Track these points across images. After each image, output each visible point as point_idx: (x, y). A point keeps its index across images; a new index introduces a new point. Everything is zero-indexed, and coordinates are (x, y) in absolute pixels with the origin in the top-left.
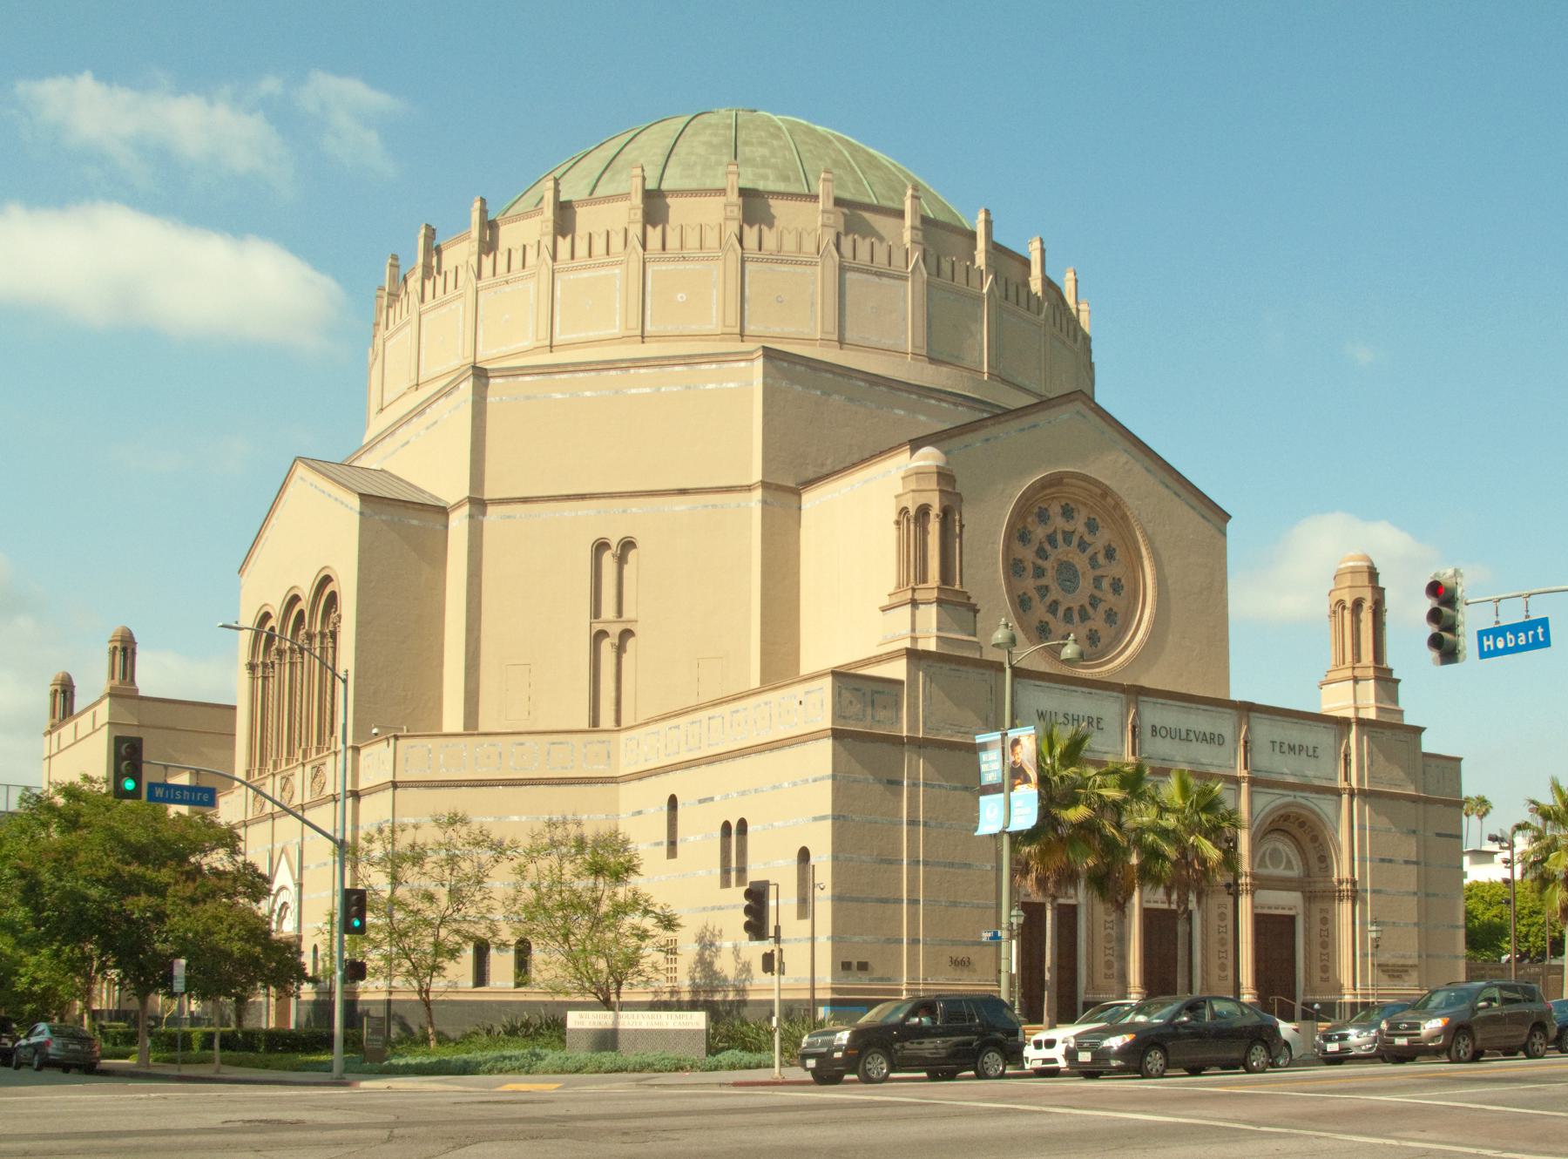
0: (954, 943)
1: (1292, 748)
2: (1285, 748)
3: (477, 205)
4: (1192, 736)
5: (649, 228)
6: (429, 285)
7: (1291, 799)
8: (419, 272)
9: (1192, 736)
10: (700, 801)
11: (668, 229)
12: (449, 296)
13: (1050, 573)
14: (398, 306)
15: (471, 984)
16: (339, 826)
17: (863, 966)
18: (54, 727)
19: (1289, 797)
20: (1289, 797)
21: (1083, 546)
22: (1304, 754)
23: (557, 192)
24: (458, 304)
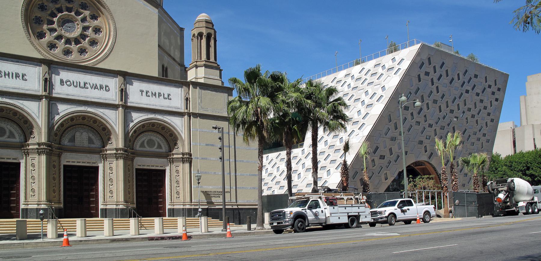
2: (150, 94)
4: (88, 85)
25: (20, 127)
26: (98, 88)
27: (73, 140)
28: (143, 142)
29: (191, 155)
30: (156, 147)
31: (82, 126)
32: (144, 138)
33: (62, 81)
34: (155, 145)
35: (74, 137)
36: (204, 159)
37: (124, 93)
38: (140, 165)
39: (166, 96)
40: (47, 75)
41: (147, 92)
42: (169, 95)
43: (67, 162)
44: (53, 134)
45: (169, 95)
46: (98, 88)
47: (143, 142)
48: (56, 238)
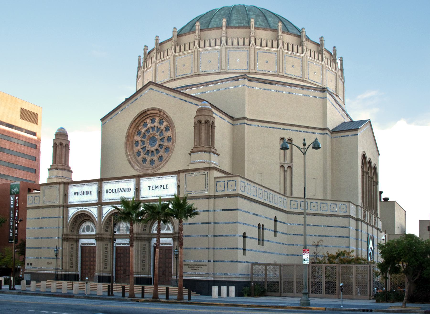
1: (157, 187)
2: (154, 187)
4: (120, 190)
7: (81, 210)
9: (120, 190)
10: (223, 210)
12: (165, 58)
13: (158, 143)
17: (31, 264)
18: (193, 204)
19: (81, 209)
20: (81, 209)
22: (162, 188)
35: (119, 227)
39: (165, 187)
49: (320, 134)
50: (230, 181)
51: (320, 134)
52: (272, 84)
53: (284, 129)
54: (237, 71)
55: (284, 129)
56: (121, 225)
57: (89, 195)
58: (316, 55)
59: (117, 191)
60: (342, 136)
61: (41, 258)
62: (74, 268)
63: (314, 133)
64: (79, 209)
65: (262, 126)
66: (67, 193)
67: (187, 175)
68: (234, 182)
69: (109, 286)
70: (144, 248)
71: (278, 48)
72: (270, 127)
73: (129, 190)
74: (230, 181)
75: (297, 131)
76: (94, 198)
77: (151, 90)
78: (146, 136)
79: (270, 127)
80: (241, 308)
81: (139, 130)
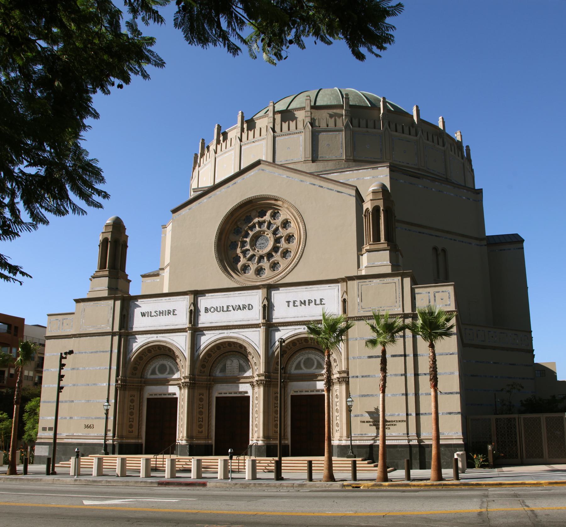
0: (87, 418)
2: (298, 303)
3: (240, 114)
4: (231, 308)
5: (283, 123)
6: (219, 147)
8: (215, 142)
9: (231, 308)
11: (298, 122)
12: (227, 150)
14: (205, 157)
15: (430, 470)
16: (42, 441)
21: (277, 240)
23: (274, 107)
24: (233, 152)
25: (300, 350)
26: (240, 309)
27: (223, 370)
28: (300, 362)
29: (348, 374)
30: (315, 366)
31: (232, 353)
32: (301, 357)
33: (207, 310)
34: (313, 365)
35: (225, 366)
36: (366, 376)
37: (268, 309)
38: (297, 392)
39: (318, 302)
40: (265, 301)
41: (294, 302)
42: (321, 300)
43: (219, 394)
44: (198, 365)
45: (174, 311)
46: (240, 309)
47: (300, 362)
48: (171, 478)
49: (478, 245)
50: (438, 292)
51: (478, 245)
52: (419, 178)
53: (436, 236)
54: (367, 159)
55: (436, 236)
56: (229, 362)
57: (171, 316)
58: (456, 151)
59: (225, 309)
60: (501, 250)
61: (71, 418)
62: (136, 433)
63: (470, 243)
64: (295, 329)
65: (410, 230)
66: (128, 314)
67: (360, 284)
68: (436, 294)
69: (277, 462)
70: (201, 400)
71: (416, 136)
72: (420, 232)
73: (250, 307)
74: (438, 292)
75: (451, 239)
76: (183, 320)
77: (261, 171)
78: (249, 234)
79: (420, 232)
80: (519, 488)
81: (238, 227)
